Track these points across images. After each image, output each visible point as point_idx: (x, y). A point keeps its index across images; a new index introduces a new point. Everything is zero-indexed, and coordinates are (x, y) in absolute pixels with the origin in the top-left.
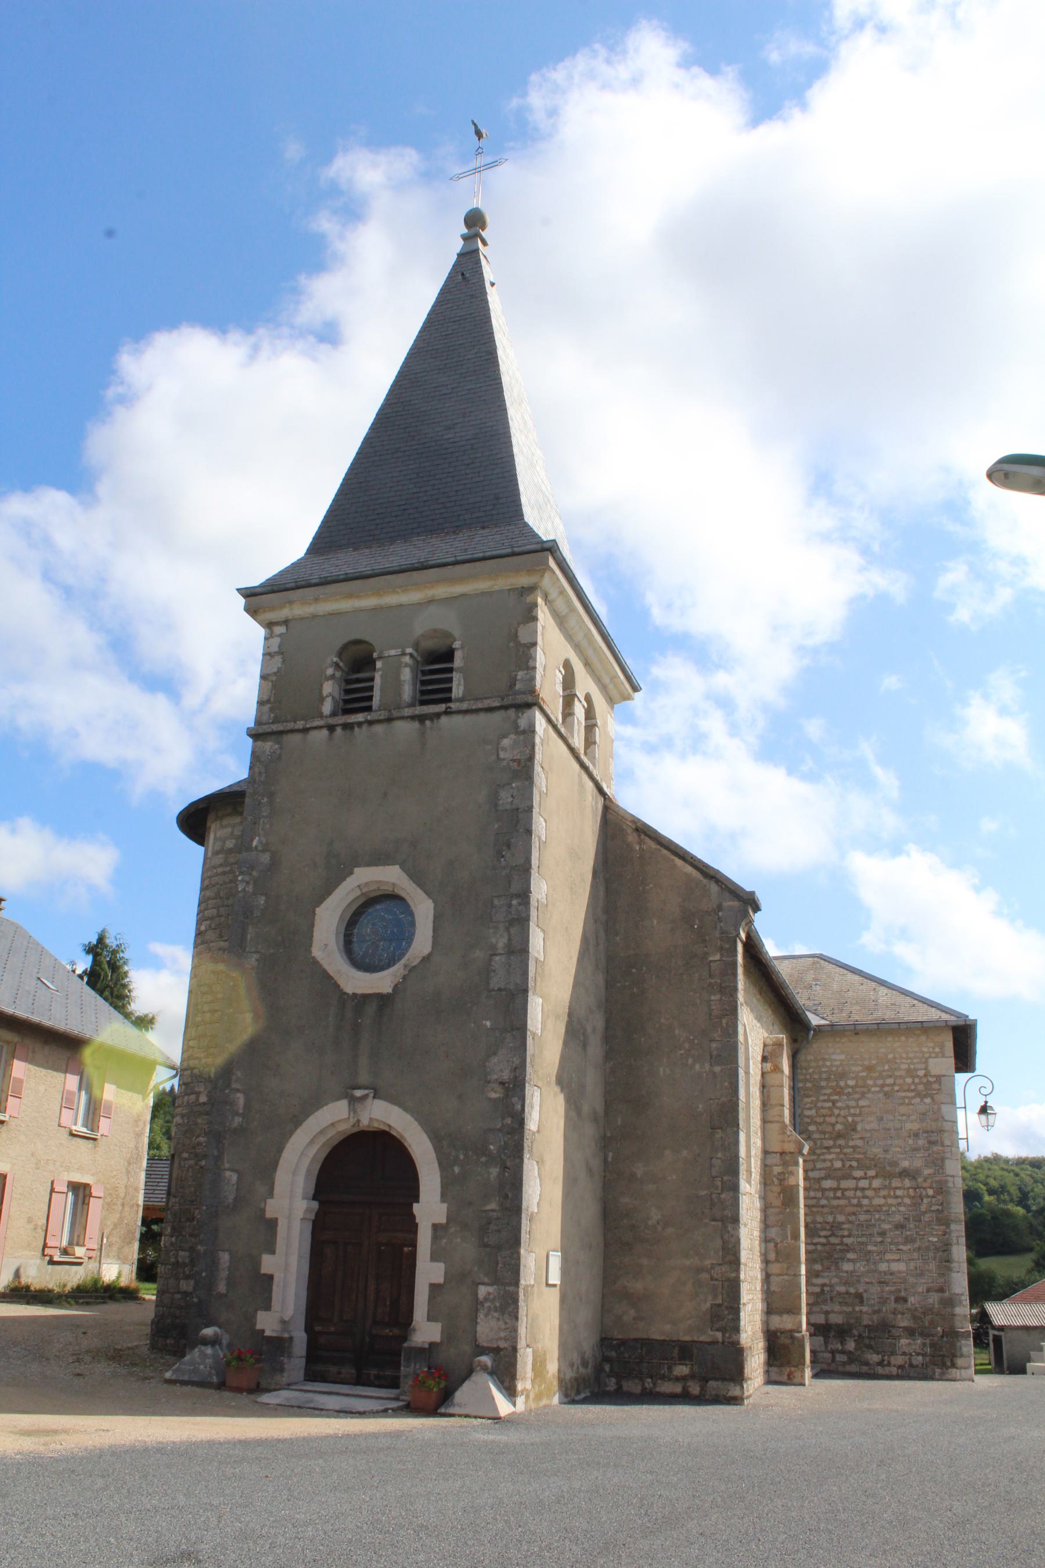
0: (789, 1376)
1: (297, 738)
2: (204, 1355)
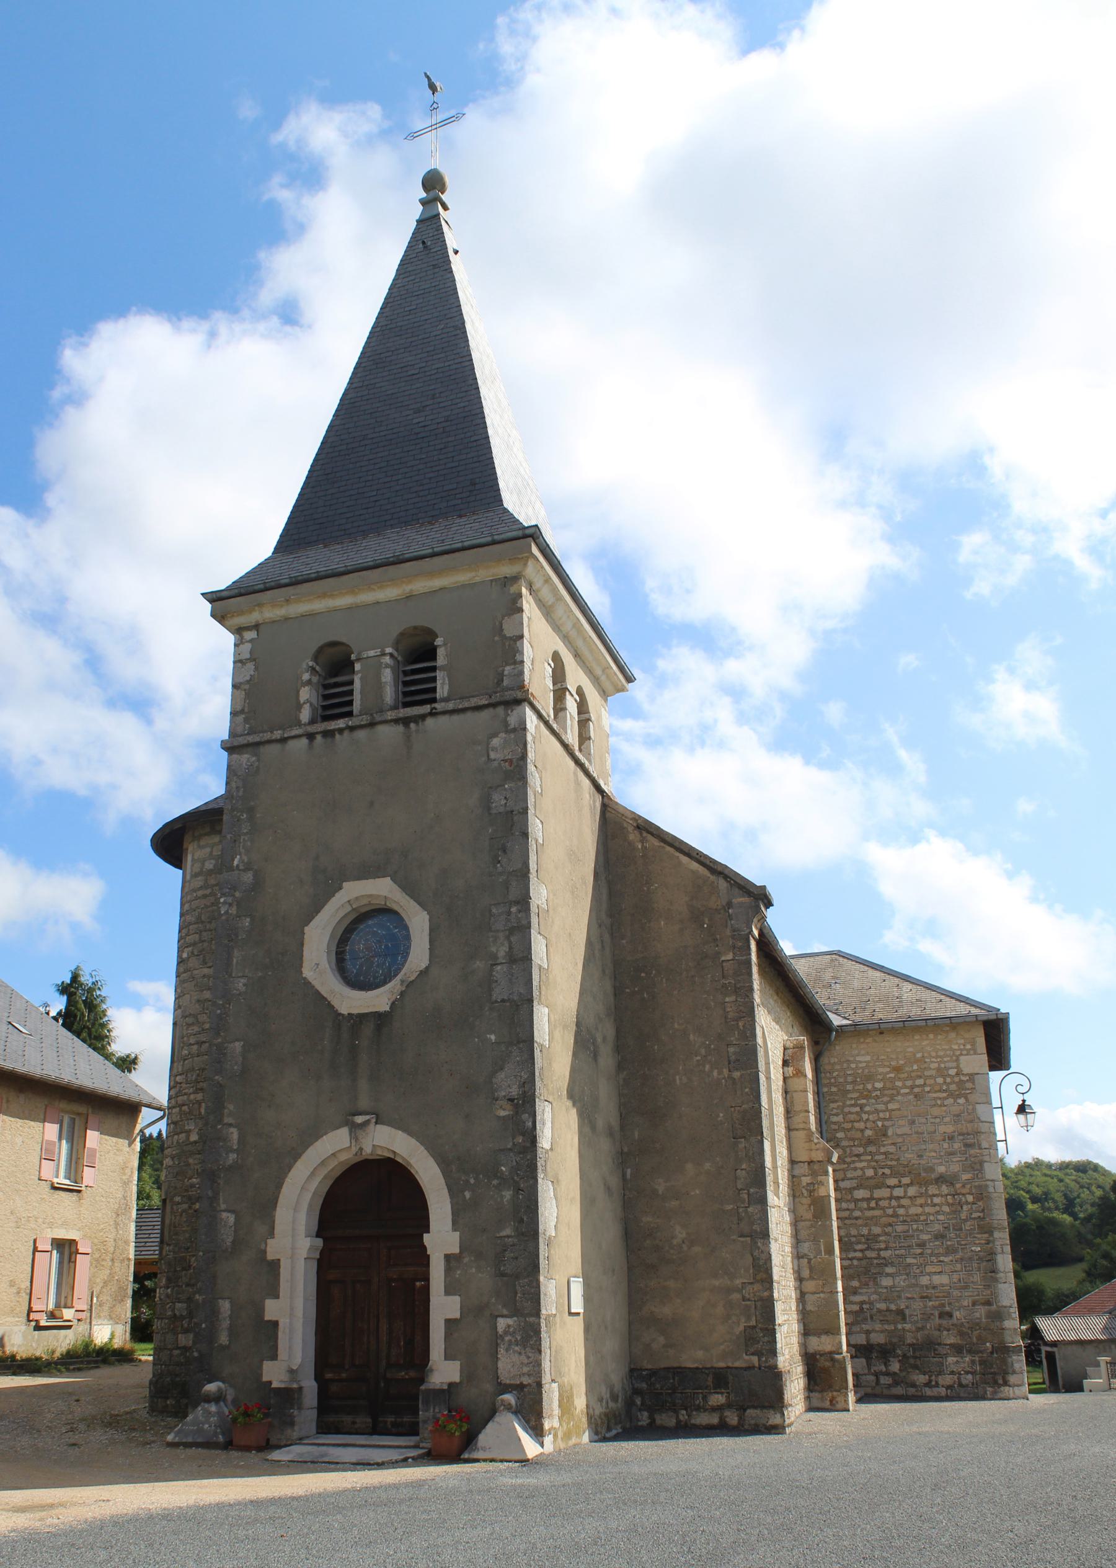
0: (831, 1401)
1: (274, 748)
2: (208, 1413)
